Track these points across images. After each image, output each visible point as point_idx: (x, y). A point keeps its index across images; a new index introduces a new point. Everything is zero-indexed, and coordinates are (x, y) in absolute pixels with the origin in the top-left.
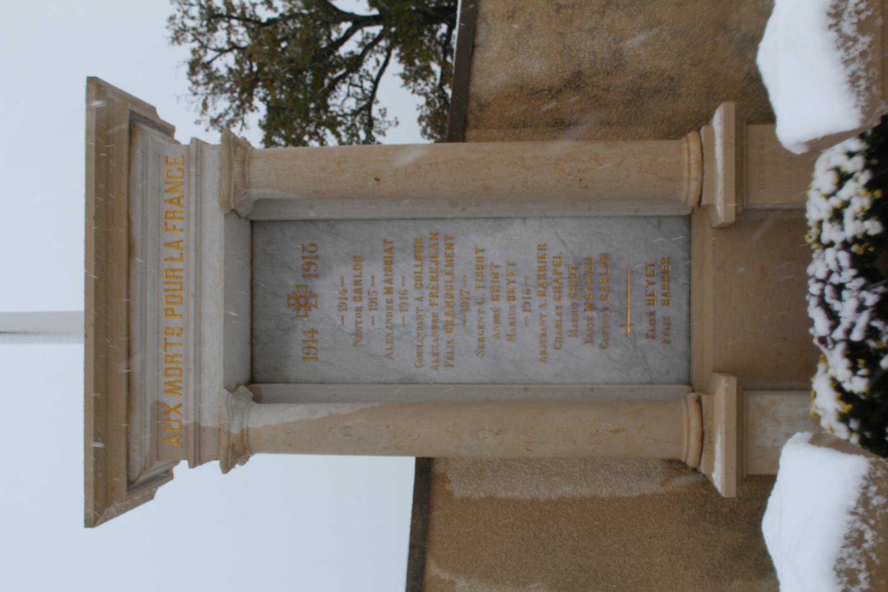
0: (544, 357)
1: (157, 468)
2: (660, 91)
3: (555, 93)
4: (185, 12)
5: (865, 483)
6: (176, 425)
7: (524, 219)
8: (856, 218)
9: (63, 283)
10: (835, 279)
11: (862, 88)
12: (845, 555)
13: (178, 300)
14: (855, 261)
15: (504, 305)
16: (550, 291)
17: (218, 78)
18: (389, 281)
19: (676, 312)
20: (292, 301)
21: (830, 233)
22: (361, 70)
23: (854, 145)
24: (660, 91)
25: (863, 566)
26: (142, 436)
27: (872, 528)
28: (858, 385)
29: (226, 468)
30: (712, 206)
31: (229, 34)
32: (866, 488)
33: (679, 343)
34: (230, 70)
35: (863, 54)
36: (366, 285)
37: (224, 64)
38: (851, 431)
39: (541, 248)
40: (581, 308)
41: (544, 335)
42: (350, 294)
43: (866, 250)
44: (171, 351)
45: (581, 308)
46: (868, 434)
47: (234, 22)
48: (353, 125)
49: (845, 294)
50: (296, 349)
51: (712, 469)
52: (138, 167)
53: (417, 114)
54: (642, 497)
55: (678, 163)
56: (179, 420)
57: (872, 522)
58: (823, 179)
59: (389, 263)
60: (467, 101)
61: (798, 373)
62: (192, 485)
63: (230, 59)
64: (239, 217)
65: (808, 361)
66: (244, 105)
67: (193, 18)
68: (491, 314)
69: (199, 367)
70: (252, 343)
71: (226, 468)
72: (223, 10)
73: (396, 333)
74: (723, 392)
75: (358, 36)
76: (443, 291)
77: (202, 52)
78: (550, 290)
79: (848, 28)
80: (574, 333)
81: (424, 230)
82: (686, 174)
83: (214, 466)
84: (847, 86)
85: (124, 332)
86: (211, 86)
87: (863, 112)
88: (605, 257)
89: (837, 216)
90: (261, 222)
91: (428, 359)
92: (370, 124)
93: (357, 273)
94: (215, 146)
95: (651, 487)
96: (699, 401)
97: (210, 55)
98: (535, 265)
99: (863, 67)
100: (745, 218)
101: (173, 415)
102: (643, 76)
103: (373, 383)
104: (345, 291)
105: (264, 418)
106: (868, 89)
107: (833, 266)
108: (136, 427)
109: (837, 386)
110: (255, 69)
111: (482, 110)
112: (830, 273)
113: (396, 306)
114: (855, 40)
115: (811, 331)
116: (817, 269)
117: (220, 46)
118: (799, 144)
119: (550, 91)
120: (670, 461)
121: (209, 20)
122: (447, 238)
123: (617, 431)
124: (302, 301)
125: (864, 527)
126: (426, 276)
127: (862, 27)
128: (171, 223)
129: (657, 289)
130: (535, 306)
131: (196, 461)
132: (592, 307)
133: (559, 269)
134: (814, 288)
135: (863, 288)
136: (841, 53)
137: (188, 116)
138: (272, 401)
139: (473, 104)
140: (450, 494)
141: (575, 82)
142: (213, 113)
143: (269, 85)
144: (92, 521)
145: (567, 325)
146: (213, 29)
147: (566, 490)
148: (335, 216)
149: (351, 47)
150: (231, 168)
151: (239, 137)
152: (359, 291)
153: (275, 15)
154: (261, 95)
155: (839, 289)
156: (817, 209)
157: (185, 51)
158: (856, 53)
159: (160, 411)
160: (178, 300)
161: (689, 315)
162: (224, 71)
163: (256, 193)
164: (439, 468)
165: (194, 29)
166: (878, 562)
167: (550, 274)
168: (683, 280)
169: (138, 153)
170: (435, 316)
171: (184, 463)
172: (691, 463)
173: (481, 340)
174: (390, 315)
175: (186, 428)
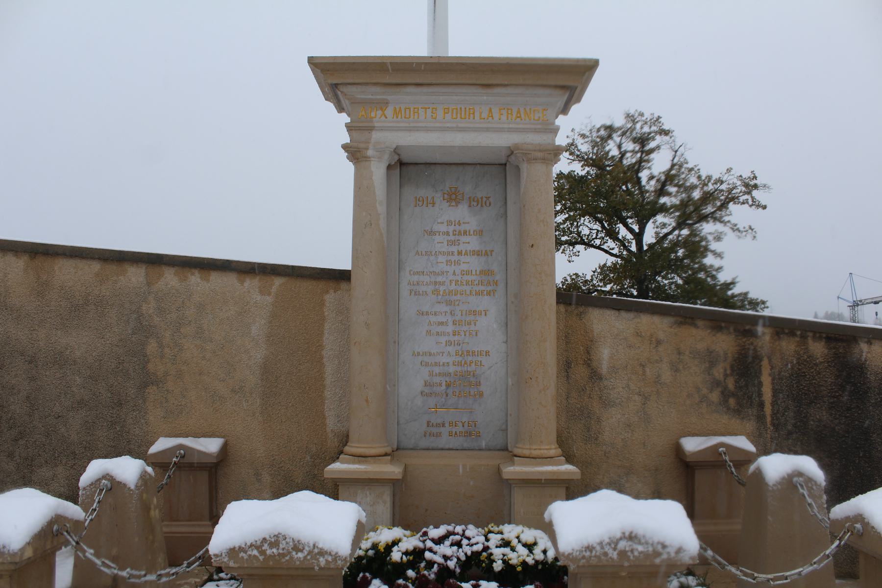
0: (416, 354)
1: (345, 103)
2: (589, 431)
3: (588, 363)
5: (333, 553)
6: (373, 115)
7: (506, 342)
8: (504, 555)
9: (466, 43)
10: (465, 542)
11: (584, 553)
12: (288, 540)
13: (454, 116)
15: (450, 328)
17: (602, 144)
18: (466, 254)
19: (444, 441)
20: (453, 190)
21: (495, 539)
23: (551, 554)
24: (589, 431)
25: (281, 551)
26: (373, 93)
27: (305, 557)
28: (396, 555)
29: (345, 147)
30: (513, 464)
32: (330, 554)
33: (424, 443)
34: (608, 152)
35: (606, 554)
36: (464, 239)
38: (367, 551)
39: (487, 353)
40: (447, 379)
41: (430, 354)
42: (457, 228)
43: (483, 561)
44: (421, 112)
45: (447, 379)
46: (364, 561)
47: (639, 155)
48: (571, 233)
49: (455, 548)
50: (423, 192)
51: (342, 463)
52: (541, 91)
54: (324, 418)
55: (541, 442)
57: (309, 557)
58: (529, 535)
59: (478, 253)
61: (404, 518)
62: (334, 125)
63: (615, 152)
64: (509, 156)
65: (412, 525)
66: (586, 161)
67: (642, 128)
68: (444, 320)
69: (410, 130)
70: (426, 164)
71: (345, 147)
72: (647, 148)
73: (432, 258)
74: (393, 470)
75: (629, 236)
76: (459, 288)
78: (460, 359)
79: (622, 545)
80: (431, 374)
81: (499, 277)
82: (535, 447)
83: (347, 139)
84: (586, 544)
85: (434, 82)
86: (598, 140)
87: (569, 554)
88: (481, 395)
89: (506, 544)
90: (505, 170)
91: (415, 278)
92: (572, 244)
93: (472, 233)
94: (554, 141)
95: (331, 423)
96: (386, 455)
97: (618, 139)
99: (598, 554)
100: (508, 485)
101: (379, 112)
102: (599, 420)
103: (400, 243)
104: (459, 224)
105: (378, 171)
106: (584, 557)
107: (473, 541)
108: (373, 89)
109: (395, 543)
111: (577, 315)
112: (469, 539)
114: (615, 549)
115: (431, 527)
116: (472, 531)
117: (623, 145)
118: (551, 515)
119: (589, 359)
120: (348, 436)
121: (640, 138)
122: (494, 291)
123: (367, 401)
125: (306, 553)
126: (470, 278)
127: (623, 554)
128: (504, 112)
129: (460, 428)
131: (349, 128)
132: (448, 386)
133: (473, 365)
134: (459, 529)
135: (458, 559)
136: (607, 540)
137: (575, 125)
140: (327, 292)
141: (595, 376)
142: (579, 141)
144: (315, 64)
145: (437, 370)
146: (635, 140)
147: (329, 369)
148: (509, 218)
149: (623, 232)
150: (540, 151)
151: (561, 156)
152: (460, 233)
155: (459, 544)
156: (510, 531)
157: (619, 121)
158: (606, 550)
159: (383, 105)
160: (454, 116)
161: (442, 449)
162: (607, 148)
163: (524, 167)
164: (344, 285)
165: (635, 128)
166: (283, 560)
167: (470, 358)
168: (466, 445)
169: (548, 91)
170: (443, 283)
171: (348, 120)
172: (347, 449)
173: (427, 313)
174: (444, 253)
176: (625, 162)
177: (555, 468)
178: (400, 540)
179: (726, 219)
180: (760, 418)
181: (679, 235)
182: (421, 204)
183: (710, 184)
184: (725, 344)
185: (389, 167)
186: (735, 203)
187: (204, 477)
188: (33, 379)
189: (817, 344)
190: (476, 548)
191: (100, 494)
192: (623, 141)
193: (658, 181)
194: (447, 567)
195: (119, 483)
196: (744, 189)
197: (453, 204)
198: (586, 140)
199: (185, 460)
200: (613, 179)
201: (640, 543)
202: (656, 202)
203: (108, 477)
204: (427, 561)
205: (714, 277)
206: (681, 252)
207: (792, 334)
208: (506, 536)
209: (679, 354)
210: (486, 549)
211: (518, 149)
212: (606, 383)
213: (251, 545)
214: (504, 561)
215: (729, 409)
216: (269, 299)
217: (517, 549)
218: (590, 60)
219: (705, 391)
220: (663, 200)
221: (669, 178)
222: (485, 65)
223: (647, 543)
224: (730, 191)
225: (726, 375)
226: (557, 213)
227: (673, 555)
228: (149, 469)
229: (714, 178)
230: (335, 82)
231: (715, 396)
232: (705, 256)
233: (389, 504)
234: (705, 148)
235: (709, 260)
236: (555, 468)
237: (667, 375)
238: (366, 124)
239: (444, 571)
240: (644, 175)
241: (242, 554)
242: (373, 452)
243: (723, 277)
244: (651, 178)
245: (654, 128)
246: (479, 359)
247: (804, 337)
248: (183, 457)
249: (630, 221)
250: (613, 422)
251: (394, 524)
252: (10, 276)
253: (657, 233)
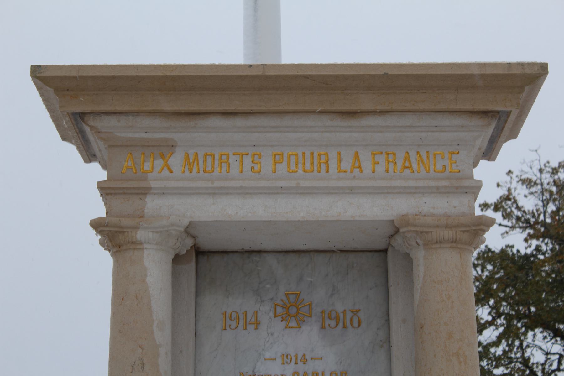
1: (97, 145)
6: (147, 166)
13: (293, 167)
20: (292, 298)
56: (153, 167)
64: (391, 237)
69: (214, 193)
71: (97, 225)
83: (99, 210)
85: (255, 108)
101: (159, 163)
105: (155, 268)
108: (147, 122)
124: (293, 310)
128: (382, 159)
131: (105, 190)
144: (42, 76)
148: (394, 349)
150: (447, 227)
154: (544, 248)
159: (164, 149)
163: (420, 256)
171: (102, 175)
175: (145, 179)
182: (234, 324)
185: (177, 259)
197: (293, 323)
198: (533, 189)
211: (408, 224)
217: (496, 331)
222: (346, 78)
226: (481, 328)
230: (79, 110)
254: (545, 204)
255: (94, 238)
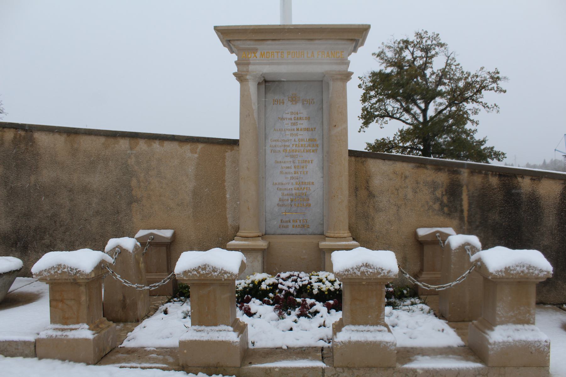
1: (234, 49)
3: (367, 188)
4: (429, 38)
6: (249, 56)
10: (299, 280)
14: (304, 286)
15: (293, 170)
16: (298, 186)
18: (301, 130)
19: (290, 230)
21: (314, 278)
22: (404, 113)
28: (264, 286)
29: (235, 74)
30: (325, 240)
31: (420, 57)
33: (279, 231)
34: (404, 57)
36: (300, 122)
37: (407, 55)
38: (249, 284)
41: (282, 184)
42: (296, 116)
47: (425, 59)
48: (381, 110)
49: (294, 283)
52: (340, 42)
53: (386, 138)
54: (227, 219)
56: (251, 56)
59: (307, 130)
60: (364, 157)
61: (268, 269)
62: (228, 60)
63: (409, 57)
65: (272, 273)
66: (390, 63)
67: (426, 41)
68: (290, 166)
71: (235, 74)
72: (429, 55)
73: (283, 132)
74: (261, 244)
75: (418, 111)
76: (298, 149)
77: (412, 45)
78: (298, 186)
79: (363, 269)
80: (283, 194)
81: (319, 142)
83: (235, 70)
88: (309, 205)
89: (320, 281)
91: (274, 143)
92: (382, 117)
95: (230, 222)
96: (259, 236)
97: (411, 49)
98: (306, 181)
101: (253, 55)
104: (297, 114)
105: (252, 87)
107: (303, 279)
108: (249, 42)
109: (263, 280)
110: (405, 68)
112: (301, 278)
113: (292, 132)
116: (302, 274)
121: (426, 49)
122: (316, 150)
124: (294, 99)
125: (218, 272)
126: (303, 143)
127: (363, 273)
129: (298, 223)
130: (292, 181)
131: (237, 63)
132: (292, 201)
134: (296, 273)
135: (295, 288)
138: (258, 89)
139: (364, 159)
140: (227, 152)
141: (371, 195)
142: (386, 51)
143: (398, 73)
145: (286, 192)
146: (422, 50)
149: (415, 109)
150: (341, 75)
153: (428, 77)
154: (394, 70)
155: (296, 281)
156: (322, 275)
157: (412, 38)
159: (255, 50)
162: (404, 54)
163: (331, 83)
164: (235, 148)
167: (303, 186)
168: (302, 232)
169: (344, 42)
170: (289, 146)
172: (238, 234)
174: (289, 130)
175: (249, 60)
176: (415, 63)
177: (347, 243)
178: (266, 279)
179: (480, 100)
180: (461, 219)
181: (450, 111)
183: (469, 78)
184: (442, 178)
185: (259, 84)
186: (485, 90)
187: (164, 249)
188: (72, 200)
189: (494, 178)
190: (304, 283)
191: (115, 255)
192: (415, 50)
193: (437, 75)
194: (290, 292)
195: (125, 250)
196: (491, 80)
199: (154, 241)
200: (407, 75)
201: (371, 268)
202: (436, 90)
203: (119, 246)
204: (279, 289)
205: (472, 138)
206: (451, 121)
207: (480, 172)
208: (320, 277)
209: (417, 183)
210: (310, 283)
212: (377, 199)
213: (194, 270)
214: (319, 289)
215: (444, 213)
216: (196, 155)
218: (366, 25)
219: (431, 203)
220: (440, 88)
221: (444, 73)
223: (374, 268)
224: (483, 81)
225: (443, 195)
227: (386, 274)
228: (138, 244)
229: (472, 74)
231: (437, 206)
232: (465, 124)
233: (260, 262)
234: (467, 55)
235: (469, 126)
236: (347, 243)
237: (410, 195)
238: (245, 62)
239: (288, 294)
240: (428, 72)
241: (189, 274)
242: (251, 235)
243: (478, 137)
244: (433, 73)
245: (434, 42)
246: (308, 186)
247: (486, 174)
248: (153, 239)
249: (419, 102)
250: (380, 221)
251: (263, 272)
252: (57, 146)
253: (436, 109)
254: (395, 55)
255: (234, 78)
